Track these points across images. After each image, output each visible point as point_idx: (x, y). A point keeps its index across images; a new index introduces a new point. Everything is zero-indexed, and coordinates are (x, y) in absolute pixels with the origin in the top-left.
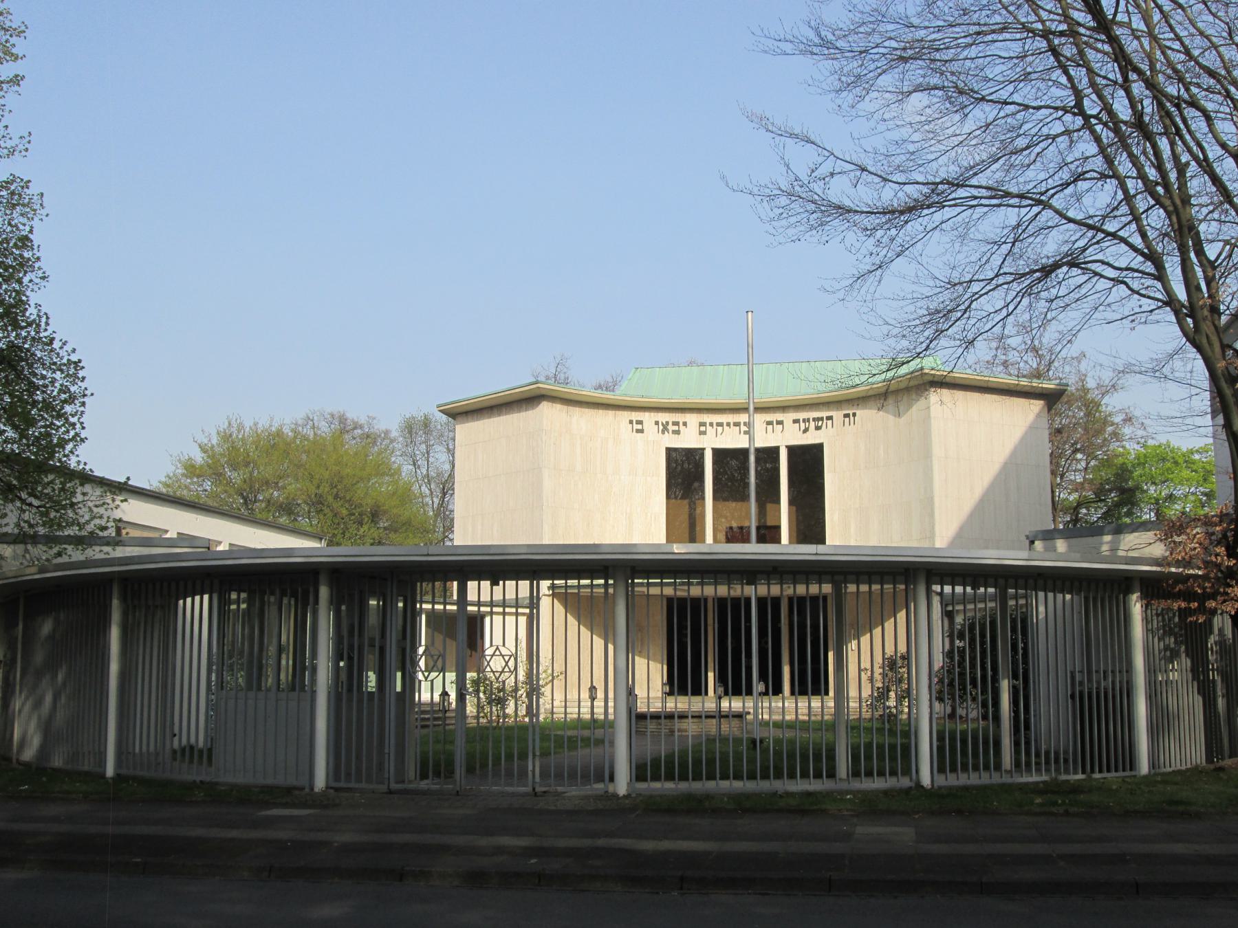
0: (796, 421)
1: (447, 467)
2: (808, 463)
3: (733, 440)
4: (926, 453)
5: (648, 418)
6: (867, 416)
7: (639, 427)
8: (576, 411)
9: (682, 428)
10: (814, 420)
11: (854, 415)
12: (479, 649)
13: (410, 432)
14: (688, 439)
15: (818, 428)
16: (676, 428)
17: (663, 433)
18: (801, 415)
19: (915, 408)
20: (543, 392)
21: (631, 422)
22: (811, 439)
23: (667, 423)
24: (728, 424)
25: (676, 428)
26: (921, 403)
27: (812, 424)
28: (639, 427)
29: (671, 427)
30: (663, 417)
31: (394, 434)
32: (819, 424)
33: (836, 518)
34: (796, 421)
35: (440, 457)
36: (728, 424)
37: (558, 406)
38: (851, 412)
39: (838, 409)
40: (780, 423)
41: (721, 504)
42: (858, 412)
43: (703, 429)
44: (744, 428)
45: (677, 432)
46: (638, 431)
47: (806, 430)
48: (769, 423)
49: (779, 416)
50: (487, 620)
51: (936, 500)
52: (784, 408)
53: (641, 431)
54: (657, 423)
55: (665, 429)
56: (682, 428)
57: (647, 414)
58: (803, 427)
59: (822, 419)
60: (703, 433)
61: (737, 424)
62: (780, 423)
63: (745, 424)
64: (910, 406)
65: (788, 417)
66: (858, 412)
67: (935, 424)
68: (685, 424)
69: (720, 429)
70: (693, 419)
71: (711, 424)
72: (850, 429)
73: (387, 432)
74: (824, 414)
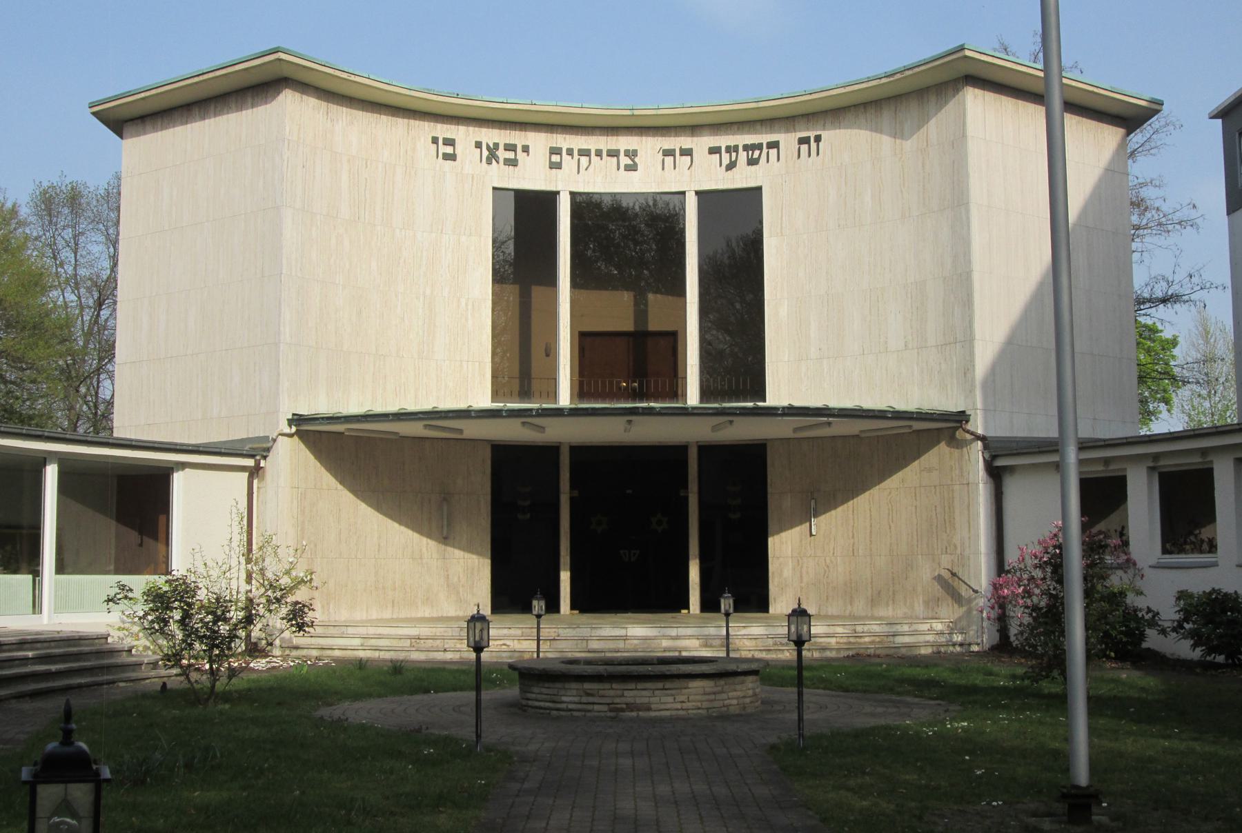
0: (714, 151)
1: (107, 264)
2: (736, 215)
3: (602, 177)
4: (956, 202)
5: (465, 136)
6: (845, 143)
7: (449, 150)
8: (343, 114)
9: (521, 156)
10: (746, 148)
11: (818, 139)
12: (162, 535)
13: (49, 211)
14: (532, 175)
15: (752, 162)
16: (511, 155)
17: (489, 163)
18: (723, 141)
19: (933, 122)
20: (287, 72)
21: (435, 140)
22: (743, 178)
23: (496, 145)
24: (599, 153)
25: (511, 155)
26: (951, 107)
27: (743, 156)
28: (449, 150)
29: (502, 154)
30: (490, 136)
31: (24, 212)
32: (754, 154)
33: (783, 311)
34: (714, 151)
35: (95, 247)
36: (599, 153)
37: (312, 101)
38: (812, 134)
39: (787, 131)
40: (687, 152)
41: (584, 294)
42: (825, 135)
43: (556, 158)
44: (625, 161)
45: (512, 163)
46: (447, 157)
47: (731, 166)
48: (668, 153)
49: (685, 142)
50: (1065, 81)
51: (976, 276)
52: (694, 128)
53: (451, 157)
54: (478, 145)
55: (492, 156)
56: (521, 156)
57: (462, 129)
58: (726, 161)
59: (759, 147)
60: (556, 166)
61: (613, 153)
62: (687, 152)
63: (627, 153)
64: (923, 121)
65: (700, 144)
66: (825, 135)
67: (975, 149)
68: (526, 149)
69: (584, 160)
70: (539, 142)
71: (570, 152)
72: (810, 163)
73: (14, 211)
74: (764, 138)
